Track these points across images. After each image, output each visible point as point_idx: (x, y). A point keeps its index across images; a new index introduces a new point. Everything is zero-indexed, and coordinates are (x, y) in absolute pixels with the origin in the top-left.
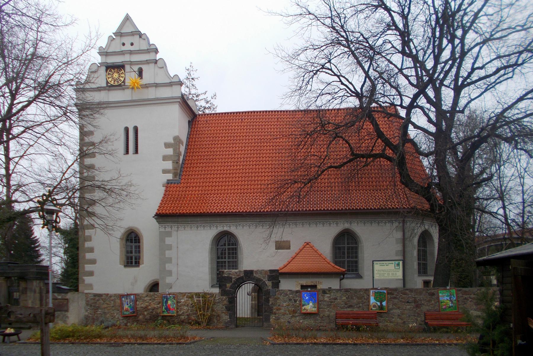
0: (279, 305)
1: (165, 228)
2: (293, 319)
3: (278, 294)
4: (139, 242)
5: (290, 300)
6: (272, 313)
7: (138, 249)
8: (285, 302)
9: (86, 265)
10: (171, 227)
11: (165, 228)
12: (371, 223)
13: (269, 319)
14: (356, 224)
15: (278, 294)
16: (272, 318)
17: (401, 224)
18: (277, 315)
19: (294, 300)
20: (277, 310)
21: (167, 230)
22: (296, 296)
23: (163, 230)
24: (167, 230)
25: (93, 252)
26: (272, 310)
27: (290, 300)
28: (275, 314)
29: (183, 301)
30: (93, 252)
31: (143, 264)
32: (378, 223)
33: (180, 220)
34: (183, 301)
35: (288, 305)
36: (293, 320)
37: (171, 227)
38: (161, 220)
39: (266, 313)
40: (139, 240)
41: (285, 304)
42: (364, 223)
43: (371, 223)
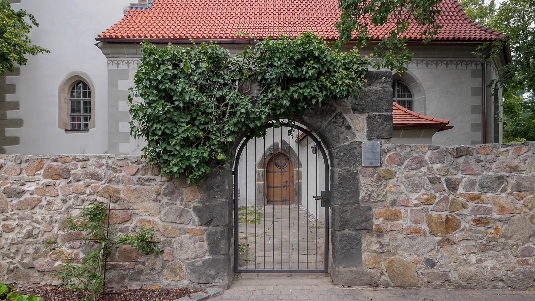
0: (394, 203)
1: (118, 64)
2: (445, 251)
3: (391, 161)
4: (90, 96)
5: (434, 181)
6: (370, 231)
7: (88, 107)
8: (416, 187)
9: (7, 129)
10: (128, 63)
11: (118, 64)
12: (437, 64)
13: (359, 252)
14: (415, 65)
15: (391, 161)
16: (369, 245)
17: (479, 67)
18: (386, 239)
19: (449, 182)
20: (387, 219)
21: (121, 67)
22: (457, 168)
23: (114, 67)
24: (121, 67)
25: (18, 109)
26: (369, 219)
27: (434, 181)
28: (380, 233)
29: (31, 187)
30: (18, 109)
31: (94, 127)
32: (447, 64)
33: (132, 45)
34: (31, 187)
35: (428, 202)
36: (445, 258)
37: (128, 63)
38: (109, 51)
39: (346, 232)
40: (90, 92)
41: (414, 198)
42: (427, 64)
43: (437, 64)
